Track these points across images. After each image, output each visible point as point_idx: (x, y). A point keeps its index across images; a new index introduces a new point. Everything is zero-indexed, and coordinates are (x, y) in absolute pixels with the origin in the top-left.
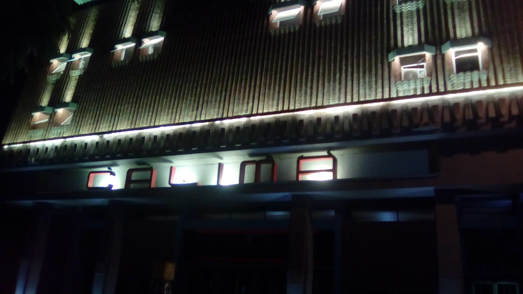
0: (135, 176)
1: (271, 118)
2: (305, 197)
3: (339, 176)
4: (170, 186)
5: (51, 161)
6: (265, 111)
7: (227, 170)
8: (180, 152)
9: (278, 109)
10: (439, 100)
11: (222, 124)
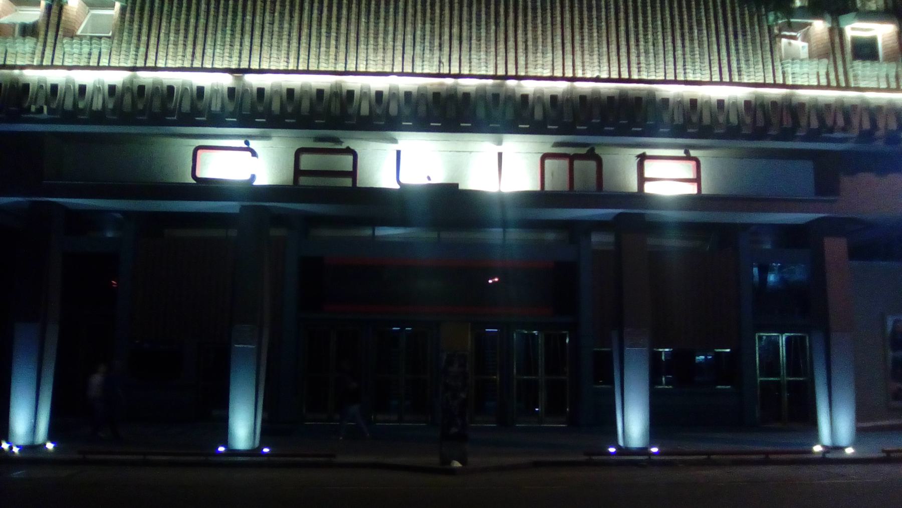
0: (308, 162)
1: (610, 89)
2: (635, 215)
3: (704, 192)
4: (398, 187)
5: (98, 117)
6: (593, 72)
7: (504, 167)
8: (172, 121)
10: (858, 98)
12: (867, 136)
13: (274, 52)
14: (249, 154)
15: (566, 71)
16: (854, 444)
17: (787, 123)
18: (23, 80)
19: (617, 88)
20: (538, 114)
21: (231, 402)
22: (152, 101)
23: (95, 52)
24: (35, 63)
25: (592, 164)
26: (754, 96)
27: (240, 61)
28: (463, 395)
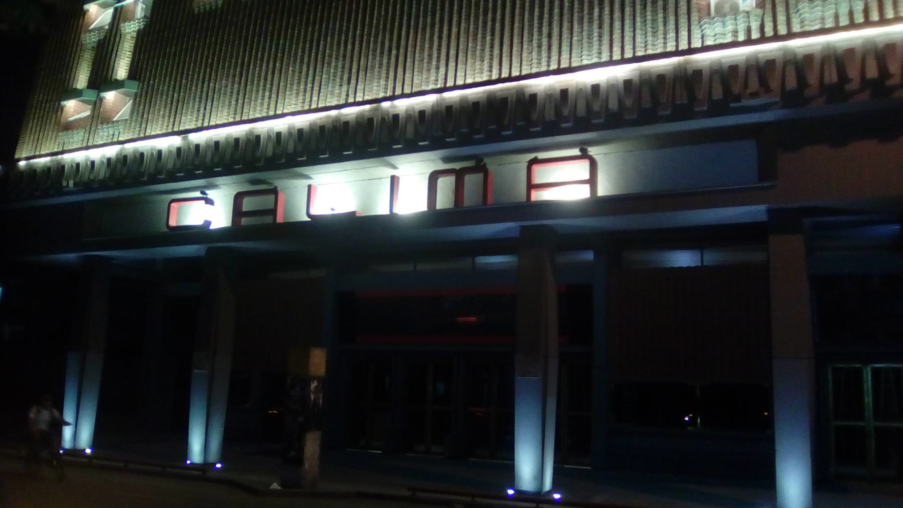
0: (248, 204)
1: (477, 94)
5: (103, 185)
6: (468, 79)
7: (406, 188)
9: (491, 76)
11: (393, 107)
12: (792, 98)
13: (478, 63)
14: (203, 202)
15: (693, 41)
16: (92, 448)
17: (682, 99)
18: (529, 91)
19: (485, 92)
20: (410, 131)
21: (777, 460)
22: (406, 127)
23: (116, 133)
24: (603, 60)
25: (480, 176)
26: (781, 53)
27: (665, 43)
28: (301, 419)
